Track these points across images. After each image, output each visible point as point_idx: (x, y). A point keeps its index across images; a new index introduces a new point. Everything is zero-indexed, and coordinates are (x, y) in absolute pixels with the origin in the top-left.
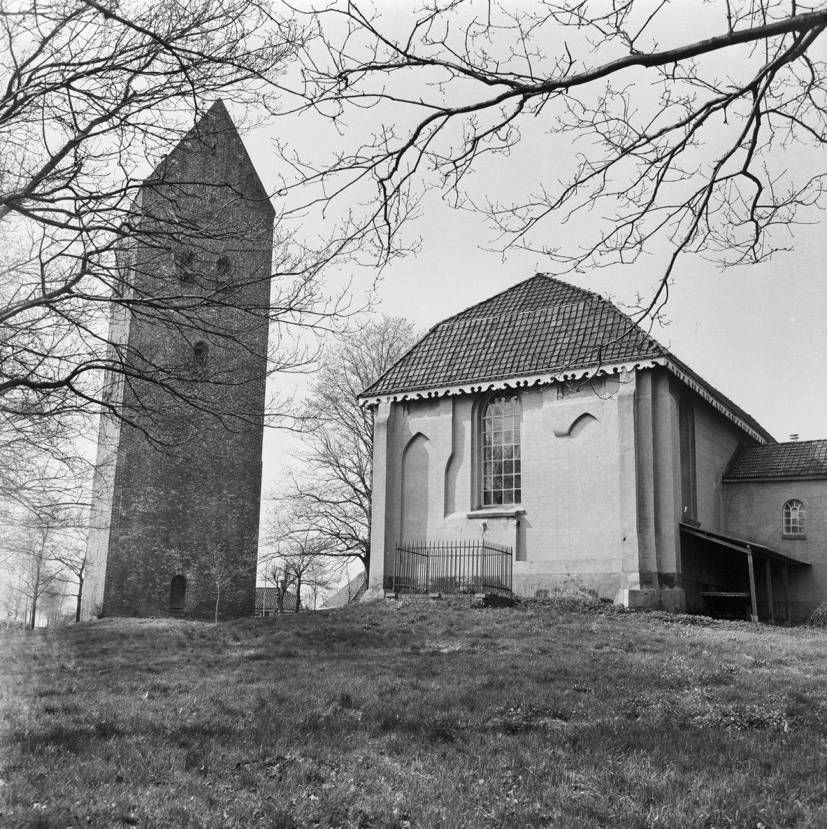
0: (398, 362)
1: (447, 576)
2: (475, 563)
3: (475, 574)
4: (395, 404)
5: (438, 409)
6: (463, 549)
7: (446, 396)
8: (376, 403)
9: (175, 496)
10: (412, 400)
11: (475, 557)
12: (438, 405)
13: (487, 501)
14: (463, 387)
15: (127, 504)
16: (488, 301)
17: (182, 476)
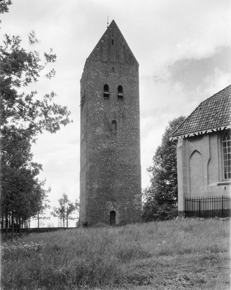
0: (185, 121)
1: (203, 210)
2: (206, 205)
3: (206, 209)
4: (185, 139)
5: (203, 139)
6: (208, 200)
7: (206, 134)
8: (177, 139)
9: (108, 181)
10: (192, 136)
11: (213, 202)
12: (203, 138)
13: (226, 178)
14: (195, 133)
15: (91, 185)
16: (224, 90)
17: (111, 173)
